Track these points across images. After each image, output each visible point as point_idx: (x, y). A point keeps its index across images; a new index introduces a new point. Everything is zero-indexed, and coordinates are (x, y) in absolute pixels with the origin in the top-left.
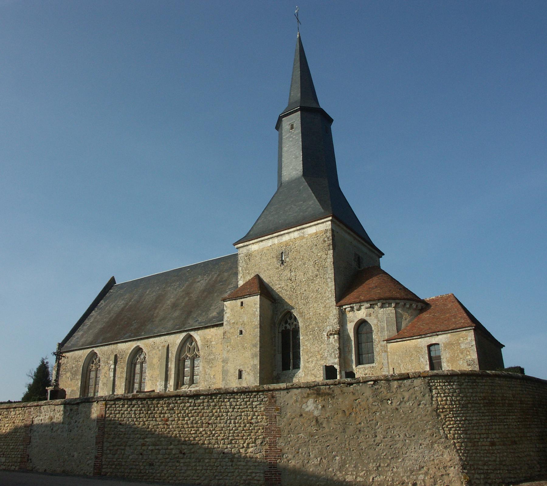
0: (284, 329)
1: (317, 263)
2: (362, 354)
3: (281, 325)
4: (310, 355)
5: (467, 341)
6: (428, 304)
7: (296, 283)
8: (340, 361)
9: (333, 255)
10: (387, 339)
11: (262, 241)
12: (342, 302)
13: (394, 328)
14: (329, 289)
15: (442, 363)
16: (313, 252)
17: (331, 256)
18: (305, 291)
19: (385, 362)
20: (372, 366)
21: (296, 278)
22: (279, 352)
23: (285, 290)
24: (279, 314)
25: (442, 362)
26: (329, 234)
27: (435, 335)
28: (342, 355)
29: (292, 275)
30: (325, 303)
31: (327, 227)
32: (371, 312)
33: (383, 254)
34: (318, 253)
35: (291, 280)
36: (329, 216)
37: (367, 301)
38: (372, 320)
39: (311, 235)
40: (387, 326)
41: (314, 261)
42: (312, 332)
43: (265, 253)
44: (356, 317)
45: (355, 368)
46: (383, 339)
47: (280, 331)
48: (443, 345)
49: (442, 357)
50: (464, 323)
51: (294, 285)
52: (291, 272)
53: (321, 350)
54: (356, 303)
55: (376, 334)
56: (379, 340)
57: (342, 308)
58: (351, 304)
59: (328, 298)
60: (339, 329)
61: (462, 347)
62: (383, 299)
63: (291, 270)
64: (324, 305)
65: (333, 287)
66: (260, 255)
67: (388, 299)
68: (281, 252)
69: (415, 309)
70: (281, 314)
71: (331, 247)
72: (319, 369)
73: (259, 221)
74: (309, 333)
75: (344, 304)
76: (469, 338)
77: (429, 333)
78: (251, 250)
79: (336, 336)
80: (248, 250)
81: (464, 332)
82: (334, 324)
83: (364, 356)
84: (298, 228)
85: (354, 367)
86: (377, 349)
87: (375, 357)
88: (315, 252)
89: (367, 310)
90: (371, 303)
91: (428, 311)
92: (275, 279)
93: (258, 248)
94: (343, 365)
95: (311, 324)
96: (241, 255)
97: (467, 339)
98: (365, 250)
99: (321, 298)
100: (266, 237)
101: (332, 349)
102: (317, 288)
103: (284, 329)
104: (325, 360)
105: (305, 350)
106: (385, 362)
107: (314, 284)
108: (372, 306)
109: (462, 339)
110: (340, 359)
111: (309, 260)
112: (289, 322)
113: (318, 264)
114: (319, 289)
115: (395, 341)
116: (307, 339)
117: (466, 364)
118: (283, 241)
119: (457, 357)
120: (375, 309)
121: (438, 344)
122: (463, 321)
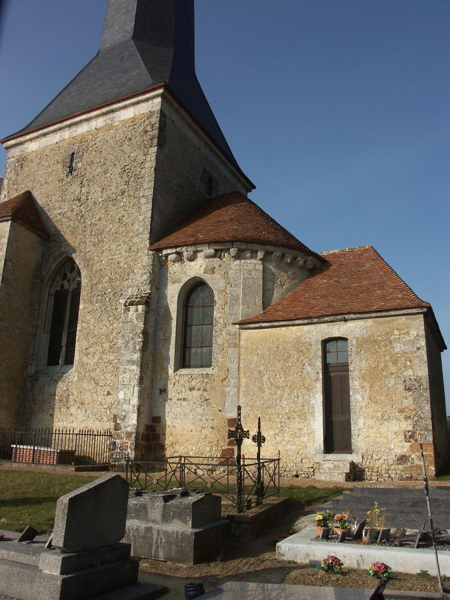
0: (59, 289)
1: (127, 171)
2: (190, 347)
3: (55, 283)
4: (92, 341)
5: (407, 338)
6: (326, 261)
7: (86, 206)
8: (142, 358)
9: (157, 155)
10: (242, 321)
11: (45, 135)
12: (163, 243)
13: (257, 300)
14: (141, 218)
15: (351, 381)
16: (123, 151)
17: (154, 158)
18: (100, 219)
19: (233, 367)
20: (205, 372)
21: (89, 197)
22: (46, 331)
23: (68, 218)
24: (52, 260)
25: (350, 377)
26: (155, 119)
27: (340, 320)
28: (150, 345)
29: (83, 191)
30: (130, 242)
31: (154, 108)
32: (215, 265)
33: (254, 187)
34: (131, 153)
35: (79, 200)
36: (159, 88)
37: (209, 243)
38: (215, 281)
39: (124, 122)
40: (245, 294)
41: (122, 166)
42: (100, 298)
43: (46, 155)
44: (186, 273)
45: (173, 375)
46: (234, 320)
47: (53, 292)
48: (354, 342)
49: (351, 368)
50: (402, 299)
51: (83, 210)
52: (82, 187)
53: (112, 333)
54: (187, 245)
55: (220, 310)
56: (225, 321)
57: (161, 255)
58: (178, 246)
59: (137, 233)
60: (150, 294)
61: (397, 350)
62: (242, 242)
63: (82, 183)
64: (128, 247)
65: (149, 214)
66: (38, 159)
67: (250, 242)
68: (71, 153)
69: (302, 268)
70: (55, 260)
71: (155, 141)
72: (105, 369)
73: (51, 107)
74: (95, 298)
75: (165, 245)
76: (414, 333)
77: (327, 316)
78: (26, 152)
79: (140, 307)
80: (23, 151)
81: (403, 318)
82: (142, 284)
83: (193, 350)
84: (104, 110)
85: (171, 371)
86: (219, 340)
87: (214, 354)
88: (126, 151)
89: (207, 260)
90: (217, 248)
91: (325, 272)
92: (54, 198)
93: (37, 147)
94: (150, 366)
95: (102, 283)
96: (11, 160)
97: (408, 333)
98: (223, 170)
99: (124, 234)
100: (52, 128)
101: (130, 333)
102: (120, 215)
103: (59, 289)
104: (117, 352)
105: (84, 331)
106: (233, 367)
107: (116, 207)
108: (217, 254)
109: (396, 332)
110: (142, 355)
111: (115, 165)
112: (68, 277)
113: (129, 172)
114: (123, 216)
115: (257, 325)
116: (91, 309)
117: (403, 388)
118: (77, 134)
119: (383, 370)
120: (224, 259)
121: (345, 339)
122: (400, 296)
